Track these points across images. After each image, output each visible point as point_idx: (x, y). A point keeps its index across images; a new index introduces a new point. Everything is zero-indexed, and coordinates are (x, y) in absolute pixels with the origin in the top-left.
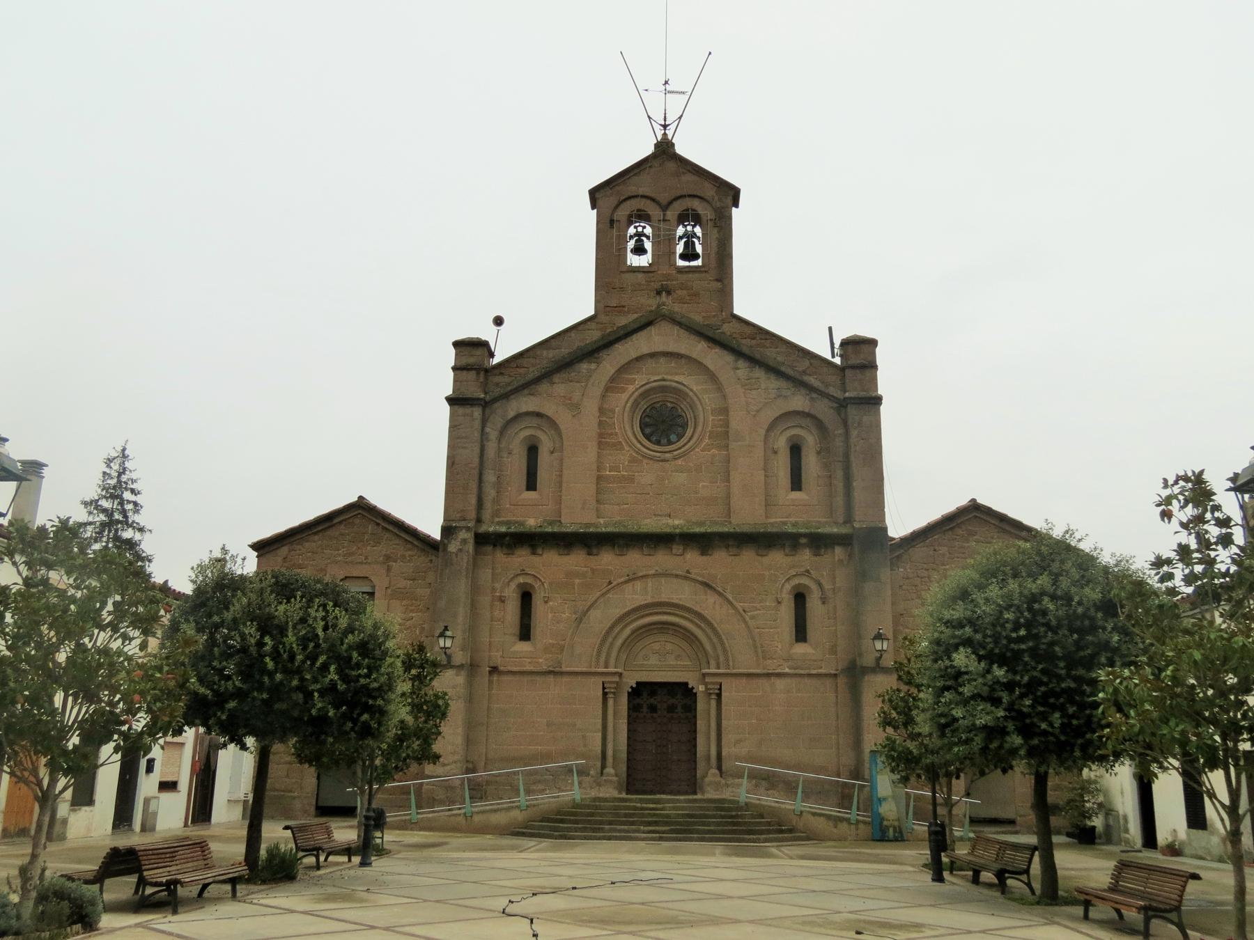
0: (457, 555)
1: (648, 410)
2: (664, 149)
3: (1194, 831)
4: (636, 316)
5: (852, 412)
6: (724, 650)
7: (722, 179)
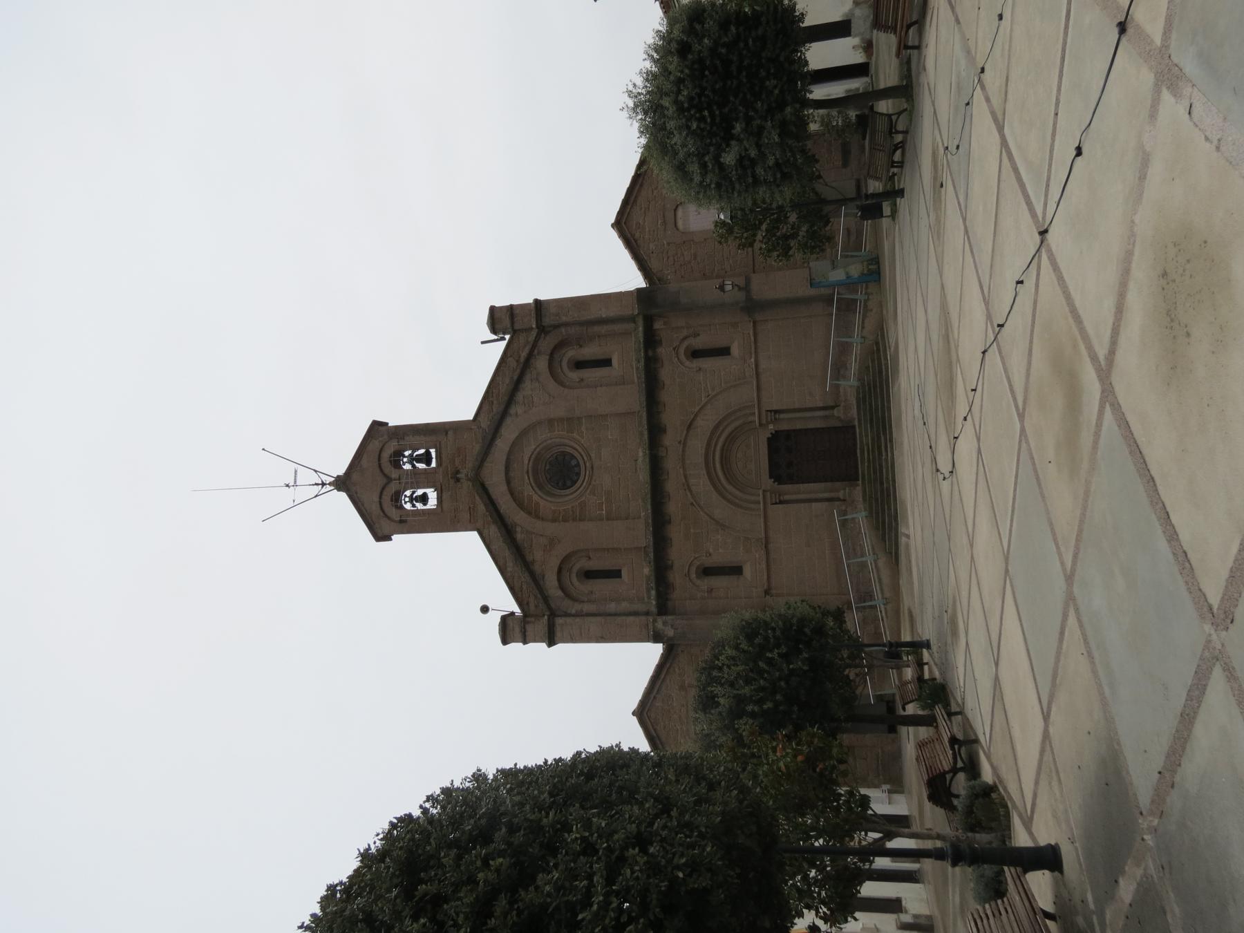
2: (341, 483)
3: (853, 30)
4: (477, 497)
5: (547, 321)
7: (366, 435)
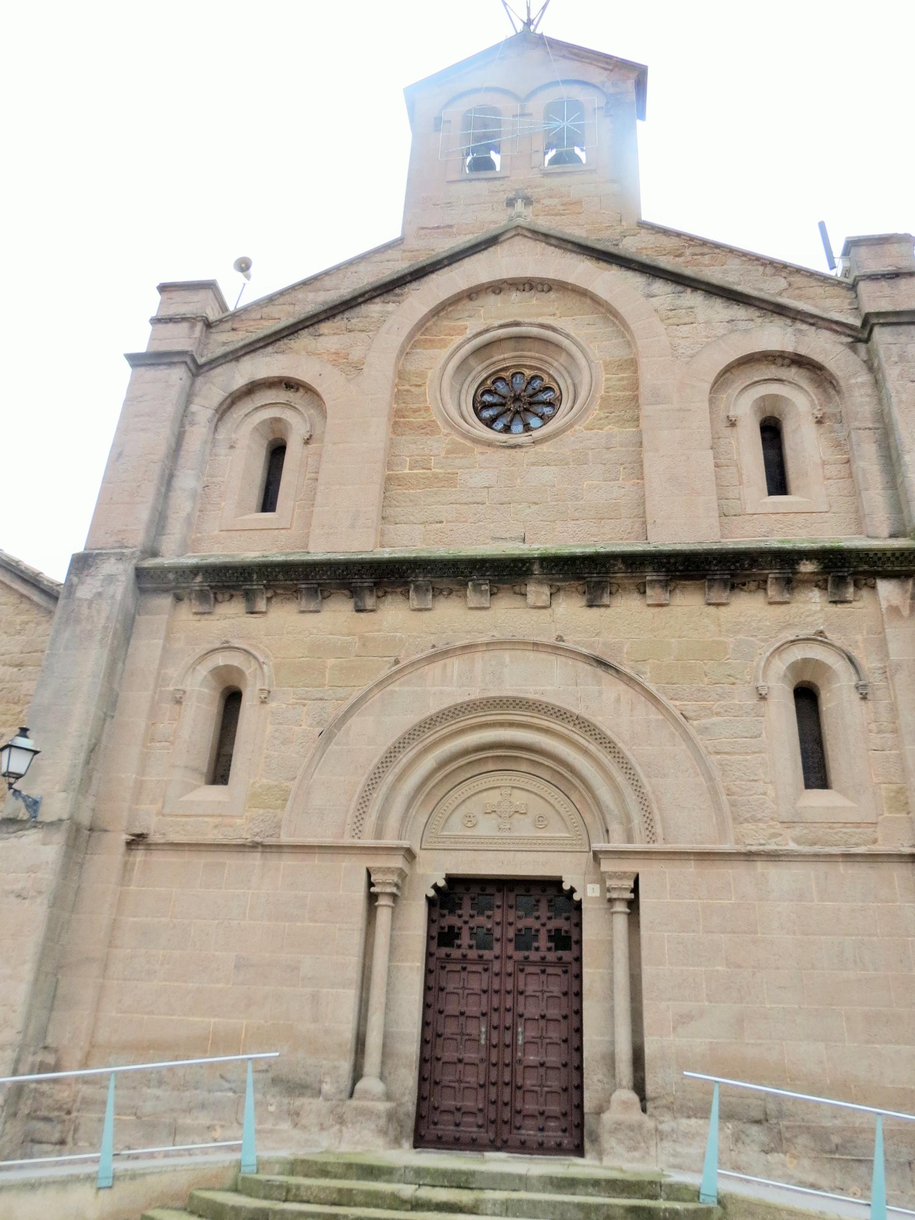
0: (90, 603)
1: (489, 382)
6: (643, 799)
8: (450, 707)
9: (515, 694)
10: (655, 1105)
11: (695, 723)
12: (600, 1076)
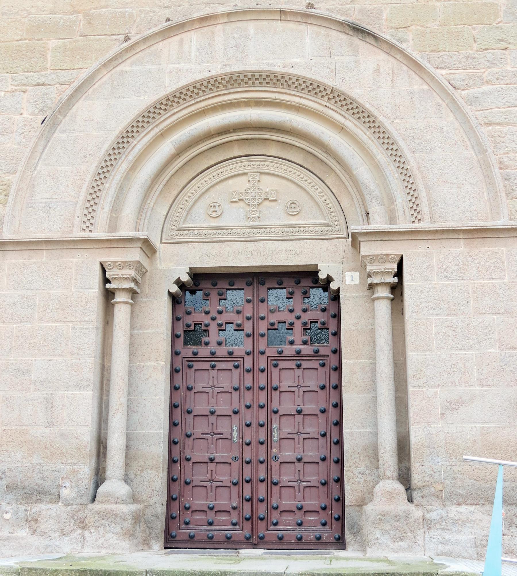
8: (188, 85)
9: (262, 68)
10: (422, 494)
11: (464, 93)
12: (362, 469)
